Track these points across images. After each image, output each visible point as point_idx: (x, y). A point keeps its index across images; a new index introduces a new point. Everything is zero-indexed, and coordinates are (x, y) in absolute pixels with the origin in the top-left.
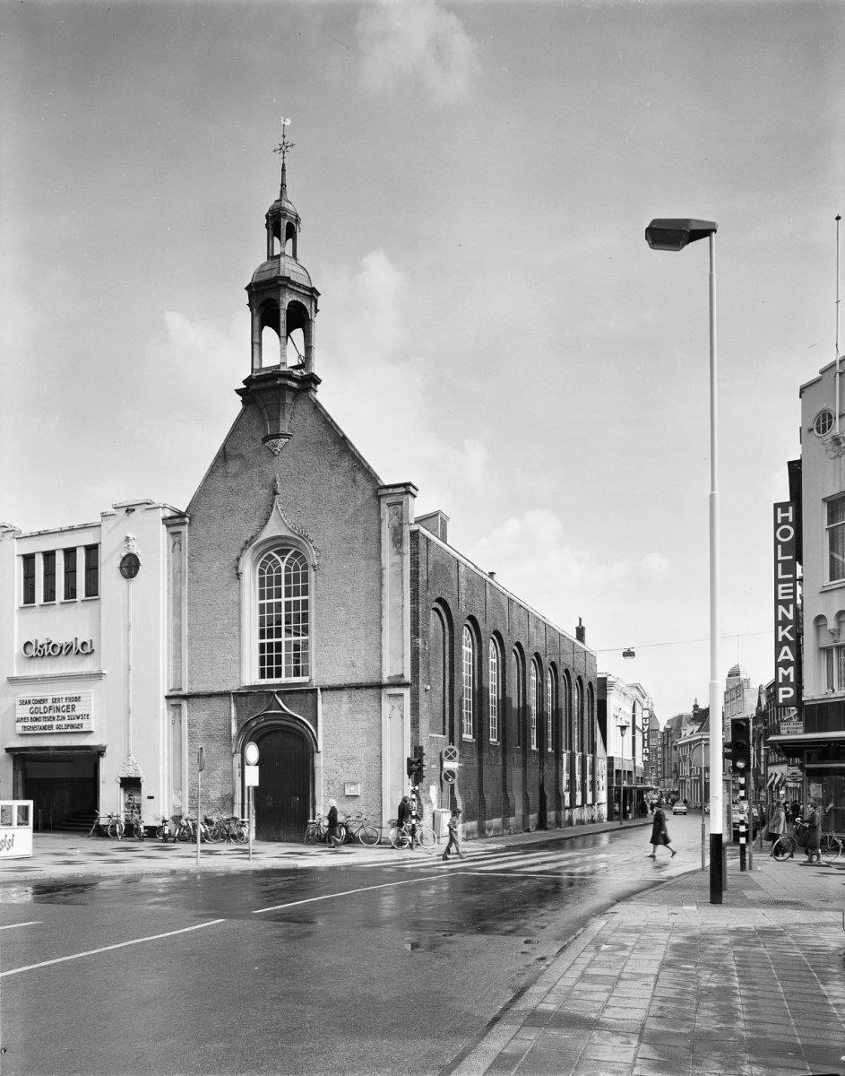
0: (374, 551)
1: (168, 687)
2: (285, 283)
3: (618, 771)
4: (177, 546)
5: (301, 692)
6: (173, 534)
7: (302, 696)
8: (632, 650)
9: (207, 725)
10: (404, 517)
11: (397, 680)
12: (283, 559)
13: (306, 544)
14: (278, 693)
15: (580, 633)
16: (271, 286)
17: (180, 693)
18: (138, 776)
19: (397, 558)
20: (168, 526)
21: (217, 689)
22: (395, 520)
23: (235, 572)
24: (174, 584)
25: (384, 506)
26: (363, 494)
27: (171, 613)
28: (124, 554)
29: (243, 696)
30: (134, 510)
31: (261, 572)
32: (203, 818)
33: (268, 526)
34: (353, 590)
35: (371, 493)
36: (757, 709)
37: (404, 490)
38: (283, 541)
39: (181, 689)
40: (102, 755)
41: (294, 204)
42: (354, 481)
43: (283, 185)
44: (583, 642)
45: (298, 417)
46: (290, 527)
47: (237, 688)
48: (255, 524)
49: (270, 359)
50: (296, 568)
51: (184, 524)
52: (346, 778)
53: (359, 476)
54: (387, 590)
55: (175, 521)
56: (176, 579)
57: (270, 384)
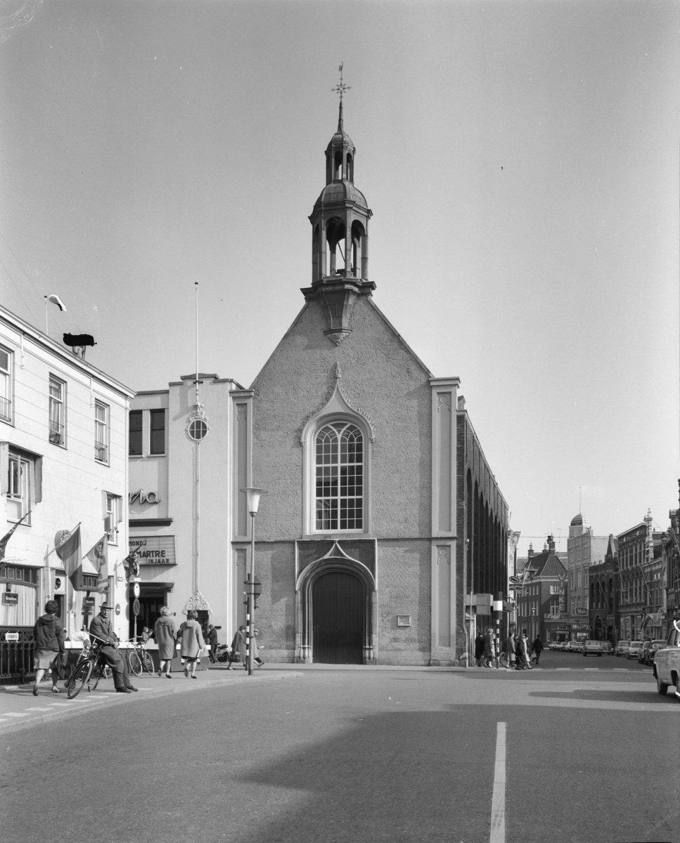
2: (351, 206)
12: (339, 431)
20: (234, 398)
25: (435, 397)
31: (318, 441)
36: (606, 556)
41: (353, 136)
43: (340, 120)
55: (240, 395)
57: (337, 288)
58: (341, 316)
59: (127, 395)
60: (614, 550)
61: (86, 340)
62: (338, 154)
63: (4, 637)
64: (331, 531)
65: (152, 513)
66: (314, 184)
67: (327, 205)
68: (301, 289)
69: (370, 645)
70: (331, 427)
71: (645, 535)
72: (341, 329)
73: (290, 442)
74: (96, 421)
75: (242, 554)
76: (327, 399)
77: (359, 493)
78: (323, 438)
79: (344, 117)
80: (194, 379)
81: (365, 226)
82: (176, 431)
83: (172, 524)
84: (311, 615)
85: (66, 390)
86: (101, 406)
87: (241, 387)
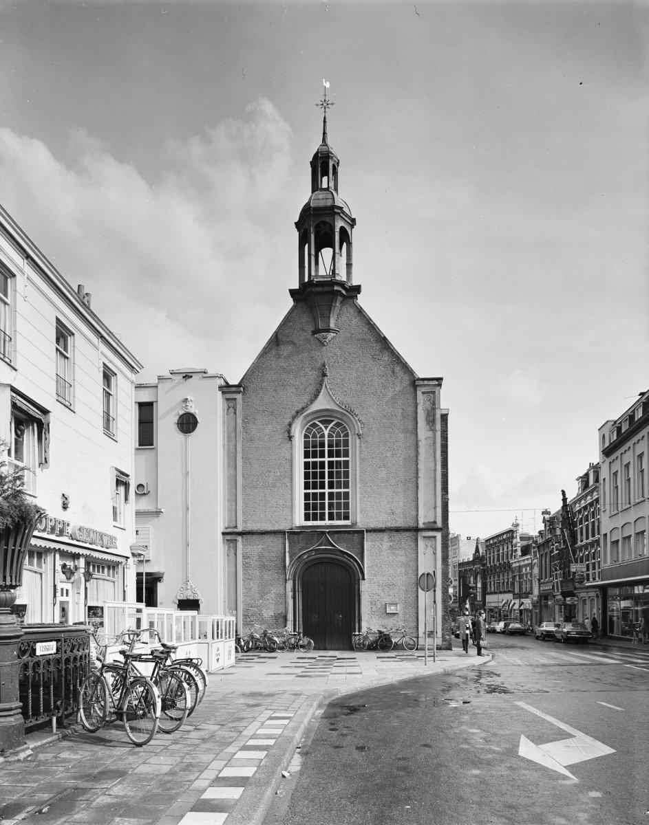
0: (410, 426)
1: (224, 525)
2: (339, 211)
4: (232, 410)
5: (348, 532)
6: (227, 399)
7: (350, 536)
8: (549, 510)
9: (261, 557)
10: (437, 403)
11: (432, 526)
12: (326, 428)
13: (352, 418)
14: (329, 533)
16: (327, 212)
17: (235, 530)
18: (197, 598)
19: (430, 434)
20: (223, 393)
21: (270, 528)
22: (428, 405)
23: (286, 435)
24: (229, 441)
25: (419, 393)
26: (402, 383)
27: (226, 465)
28: (181, 412)
29: (294, 534)
30: (191, 377)
31: (306, 436)
33: (317, 401)
34: (392, 456)
35: (408, 383)
36: (474, 555)
37: (437, 383)
38: (328, 413)
39: (236, 527)
40: (160, 581)
41: (335, 147)
42: (393, 372)
43: (324, 133)
45: (344, 318)
46: (338, 403)
47: (289, 527)
48: (306, 398)
49: (324, 270)
50: (338, 435)
51: (239, 392)
52: (387, 600)
53: (398, 369)
54: (422, 457)
55: (226, 389)
56: (232, 435)
57: (326, 289)
58: (329, 317)
59: (133, 368)
60: (481, 551)
62: (323, 164)
63: (34, 650)
67: (316, 209)
68: (290, 290)
69: (359, 632)
70: (318, 423)
71: (513, 537)
72: (330, 329)
73: (279, 437)
74: (104, 389)
75: (232, 545)
76: (316, 396)
77: (346, 486)
78: (310, 433)
79: (327, 131)
81: (350, 234)
82: (165, 426)
84: (301, 603)
85: (74, 344)
86: (108, 375)
87: (227, 383)
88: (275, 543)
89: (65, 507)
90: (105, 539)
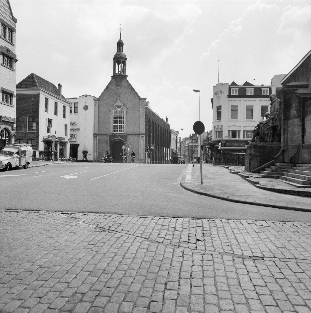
3: (173, 153)
6: (95, 102)
14: (118, 135)
15: (167, 119)
25: (140, 102)
32: (272, 143)
43: (120, 37)
44: (167, 122)
55: (95, 99)
61: (182, 130)
64: (117, 132)
65: (75, 127)
66: (114, 51)
75: (96, 138)
80: (86, 96)
83: (193, 90)
88: (195, 265)
89: (55, 133)
90: (63, 139)
